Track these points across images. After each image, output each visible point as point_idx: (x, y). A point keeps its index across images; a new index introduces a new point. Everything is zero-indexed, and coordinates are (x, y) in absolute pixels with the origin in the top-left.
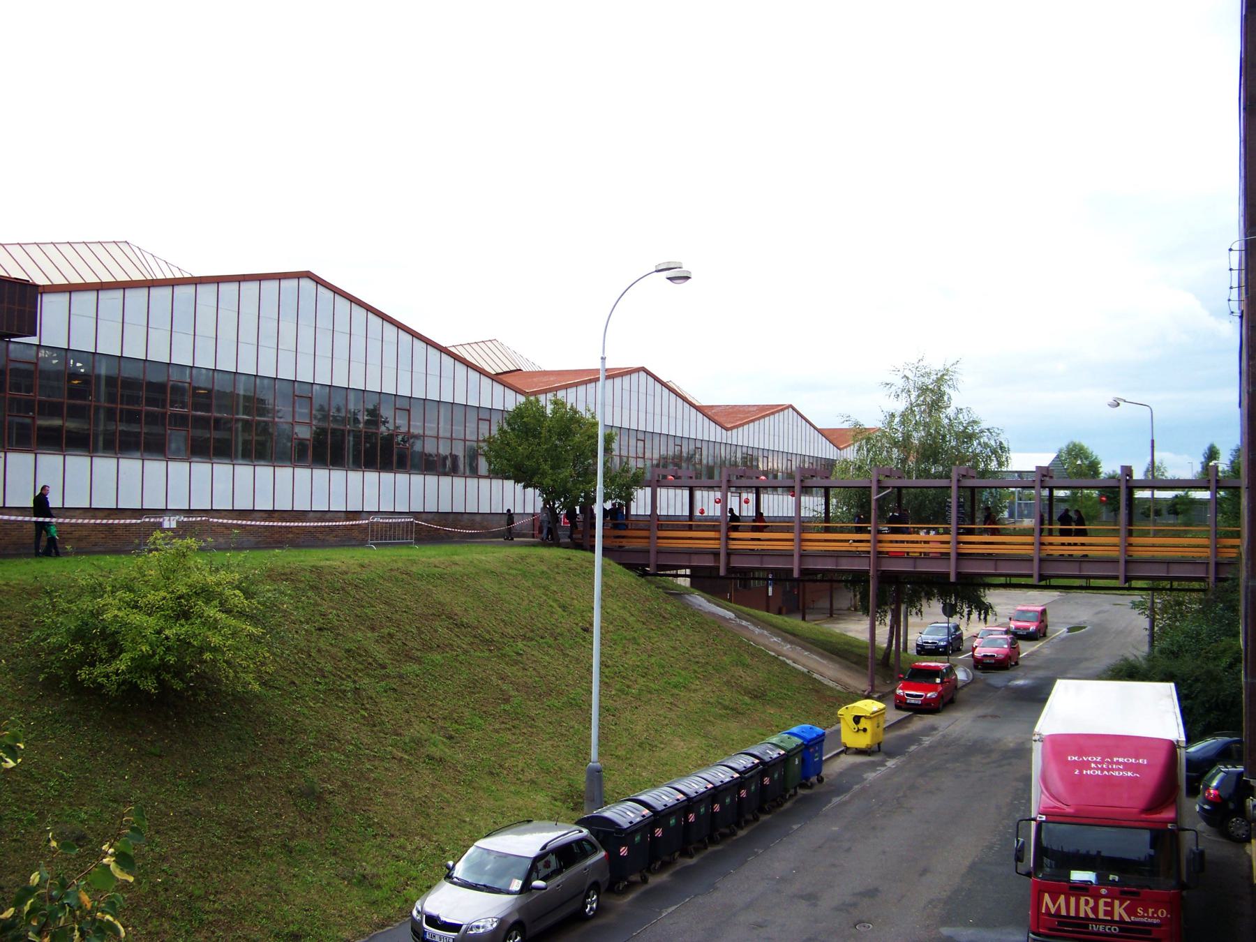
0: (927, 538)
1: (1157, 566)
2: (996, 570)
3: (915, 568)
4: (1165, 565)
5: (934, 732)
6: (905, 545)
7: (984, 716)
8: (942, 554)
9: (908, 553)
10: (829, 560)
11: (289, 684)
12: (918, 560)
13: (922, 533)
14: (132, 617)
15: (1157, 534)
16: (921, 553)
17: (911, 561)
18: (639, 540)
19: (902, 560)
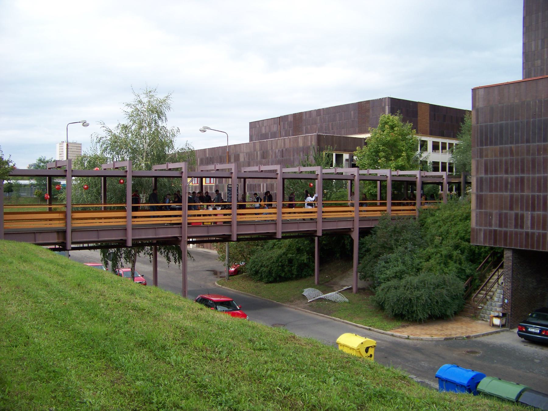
0: (215, 212)
1: (365, 222)
2: (208, 233)
3: (98, 238)
4: (33, 235)
5: (467, 196)
6: (202, 217)
7: (226, 311)
8: (225, 222)
9: (203, 223)
10: (151, 231)
11: (374, 367)
12: (210, 228)
13: (211, 209)
14: (464, 331)
15: (106, 210)
16: (211, 222)
17: (206, 228)
18: (10, 207)
19: (199, 228)
